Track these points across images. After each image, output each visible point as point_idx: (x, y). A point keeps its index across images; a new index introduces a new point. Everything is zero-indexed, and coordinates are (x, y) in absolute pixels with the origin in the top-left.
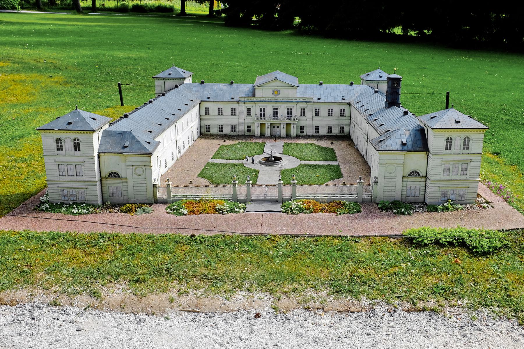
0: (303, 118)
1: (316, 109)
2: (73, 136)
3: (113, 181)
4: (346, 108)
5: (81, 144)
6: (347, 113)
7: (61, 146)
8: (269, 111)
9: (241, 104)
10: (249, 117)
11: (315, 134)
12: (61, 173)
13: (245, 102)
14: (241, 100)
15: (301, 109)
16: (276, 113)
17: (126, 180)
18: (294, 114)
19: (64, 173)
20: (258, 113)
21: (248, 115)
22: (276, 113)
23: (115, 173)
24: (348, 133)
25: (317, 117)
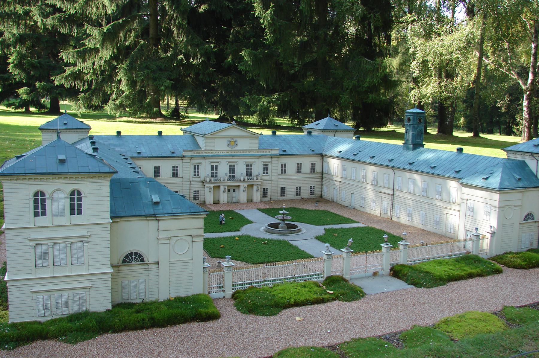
0: (266, 177)
1: (282, 165)
2: (69, 186)
3: (134, 271)
4: (316, 160)
5: (84, 202)
6: (318, 169)
7: (44, 207)
8: (223, 171)
9: (186, 161)
10: (196, 179)
11: (282, 198)
12: (39, 263)
13: (191, 158)
14: (186, 154)
15: (264, 165)
16: (232, 169)
17: (156, 266)
18: (255, 172)
19: (45, 263)
20: (209, 171)
21: (195, 175)
22: (232, 169)
23: (136, 254)
24: (320, 194)
25: (283, 175)
